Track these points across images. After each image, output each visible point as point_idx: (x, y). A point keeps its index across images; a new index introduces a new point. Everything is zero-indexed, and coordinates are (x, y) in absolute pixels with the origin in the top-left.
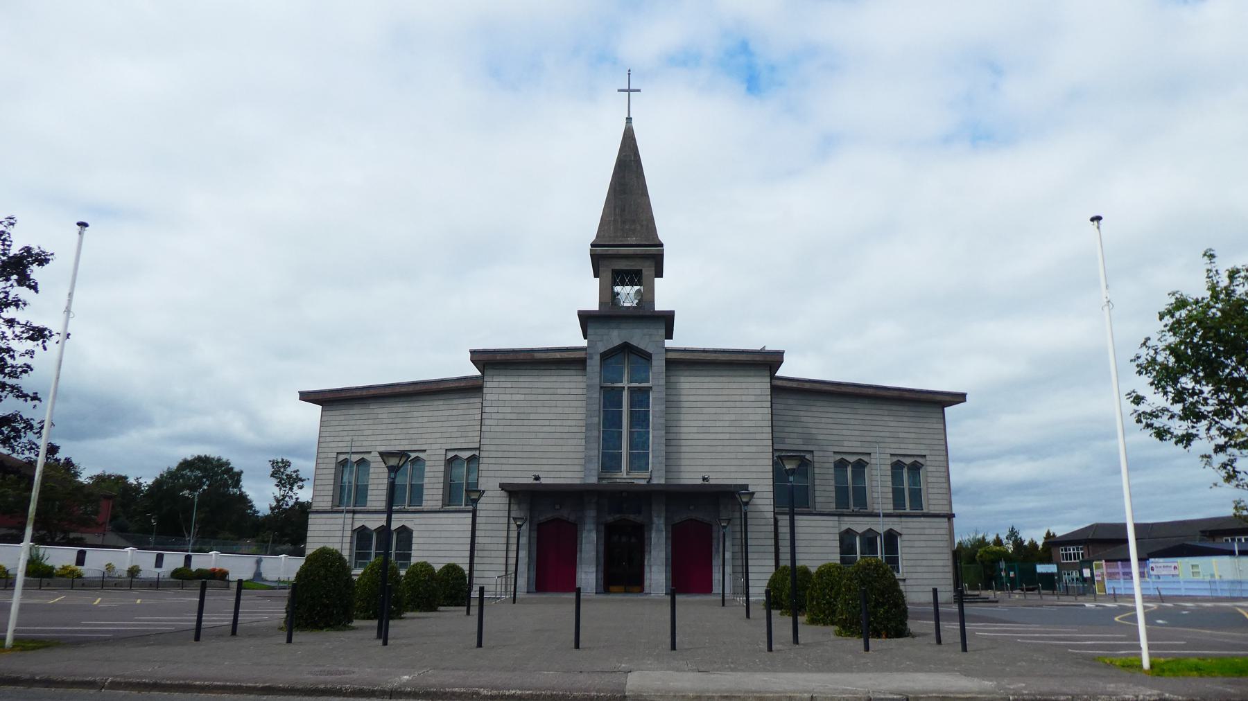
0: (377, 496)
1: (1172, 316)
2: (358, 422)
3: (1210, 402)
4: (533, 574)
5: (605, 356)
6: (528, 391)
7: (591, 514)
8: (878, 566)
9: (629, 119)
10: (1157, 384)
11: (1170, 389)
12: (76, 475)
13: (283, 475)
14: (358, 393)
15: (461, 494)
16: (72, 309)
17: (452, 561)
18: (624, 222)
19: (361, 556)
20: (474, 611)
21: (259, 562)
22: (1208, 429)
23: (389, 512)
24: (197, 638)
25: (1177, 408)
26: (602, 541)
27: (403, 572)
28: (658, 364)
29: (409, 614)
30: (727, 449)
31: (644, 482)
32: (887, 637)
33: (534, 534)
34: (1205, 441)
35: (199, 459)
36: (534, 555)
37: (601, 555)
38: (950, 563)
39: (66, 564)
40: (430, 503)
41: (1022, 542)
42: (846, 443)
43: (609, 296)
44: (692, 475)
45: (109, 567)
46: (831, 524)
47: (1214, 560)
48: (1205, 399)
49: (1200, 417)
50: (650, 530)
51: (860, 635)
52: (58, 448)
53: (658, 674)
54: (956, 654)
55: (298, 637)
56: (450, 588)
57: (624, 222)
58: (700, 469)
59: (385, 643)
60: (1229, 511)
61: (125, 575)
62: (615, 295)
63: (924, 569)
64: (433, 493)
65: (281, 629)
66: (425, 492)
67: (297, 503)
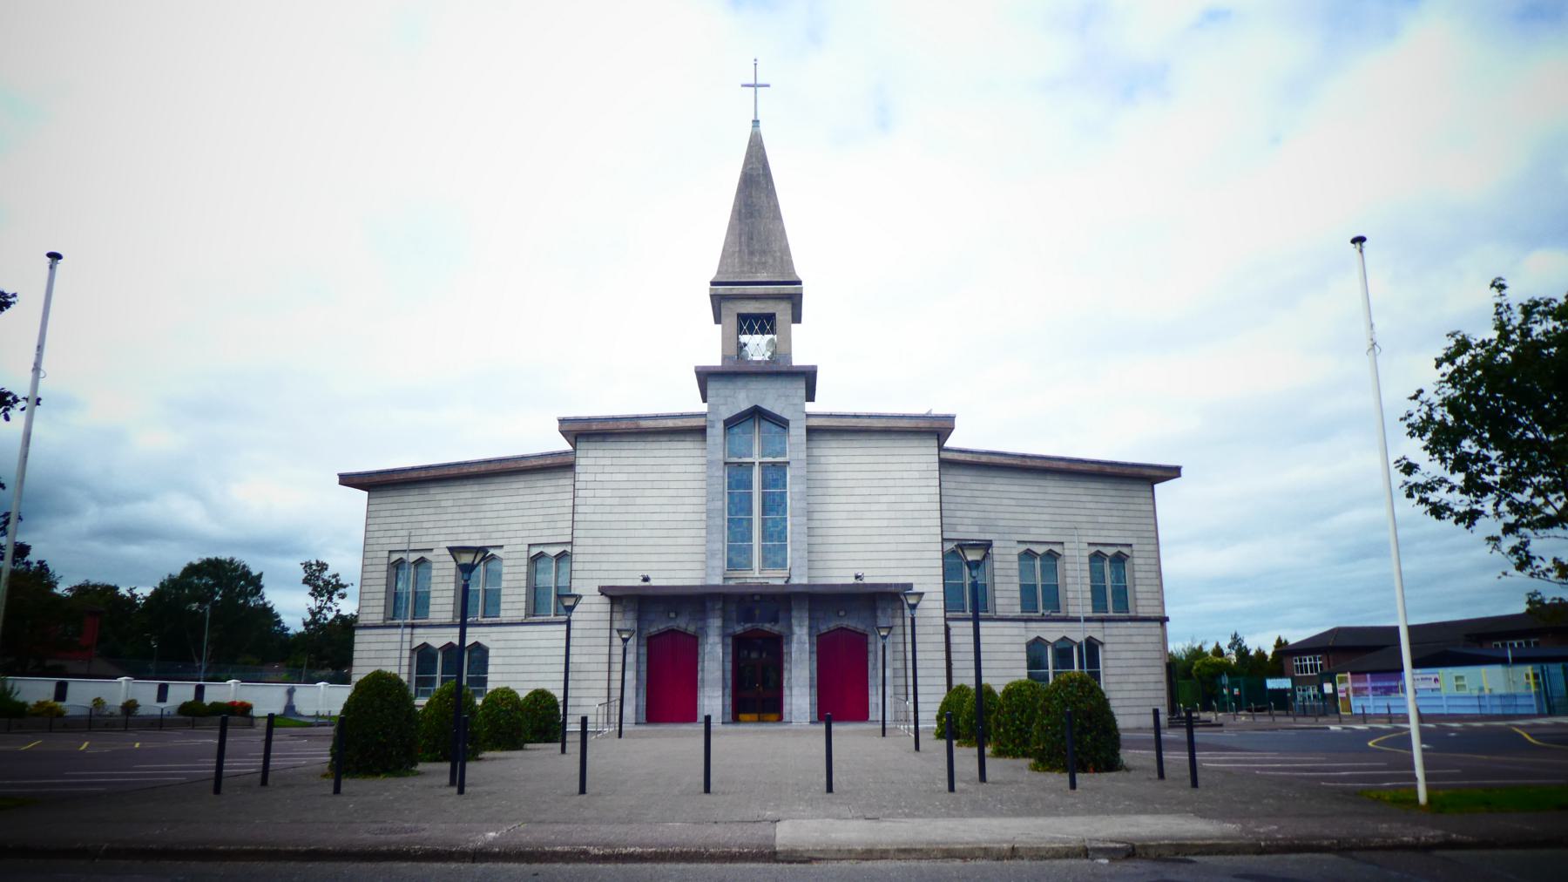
0: (442, 604)
1: (1453, 363)
2: (416, 512)
3: (1499, 470)
4: (643, 703)
5: (730, 424)
6: (632, 469)
7: (715, 623)
8: (1082, 683)
9: (756, 122)
10: (1434, 448)
11: (1448, 455)
12: (53, 585)
13: (320, 581)
14: (414, 475)
15: (551, 604)
16: (43, 366)
17: (540, 686)
18: (752, 253)
19: (424, 681)
20: (573, 746)
21: (290, 692)
22: (1497, 505)
23: (463, 627)
24: (217, 790)
25: (1458, 478)
26: (730, 658)
27: (479, 702)
28: (797, 432)
29: (487, 754)
30: (885, 539)
31: (781, 582)
32: (1095, 771)
33: (644, 650)
34: (1492, 519)
35: (209, 561)
36: (644, 675)
37: (729, 675)
38: (1164, 678)
39: (42, 699)
40: (509, 613)
41: (1247, 652)
42: (1032, 531)
43: (733, 351)
44: (843, 572)
45: (98, 702)
46: (1016, 631)
47: (1483, 670)
48: (1493, 467)
49: (1486, 489)
50: (790, 642)
51: (1065, 769)
52: (28, 548)
53: (815, 823)
54: (1185, 792)
55: (348, 784)
56: (538, 720)
57: (752, 253)
58: (851, 564)
59: (461, 791)
60: (1521, 608)
61: (118, 712)
62: (741, 347)
63: (1132, 686)
64: (513, 602)
65: (325, 776)
66: (503, 599)
67: (338, 616)
